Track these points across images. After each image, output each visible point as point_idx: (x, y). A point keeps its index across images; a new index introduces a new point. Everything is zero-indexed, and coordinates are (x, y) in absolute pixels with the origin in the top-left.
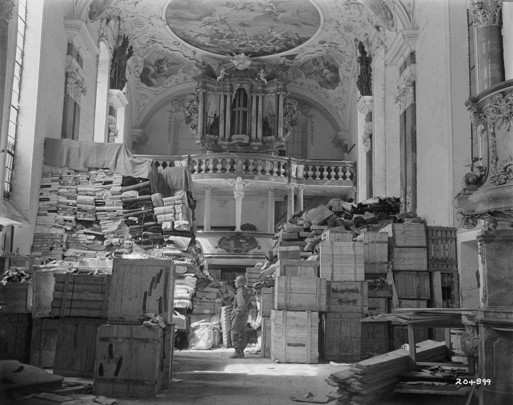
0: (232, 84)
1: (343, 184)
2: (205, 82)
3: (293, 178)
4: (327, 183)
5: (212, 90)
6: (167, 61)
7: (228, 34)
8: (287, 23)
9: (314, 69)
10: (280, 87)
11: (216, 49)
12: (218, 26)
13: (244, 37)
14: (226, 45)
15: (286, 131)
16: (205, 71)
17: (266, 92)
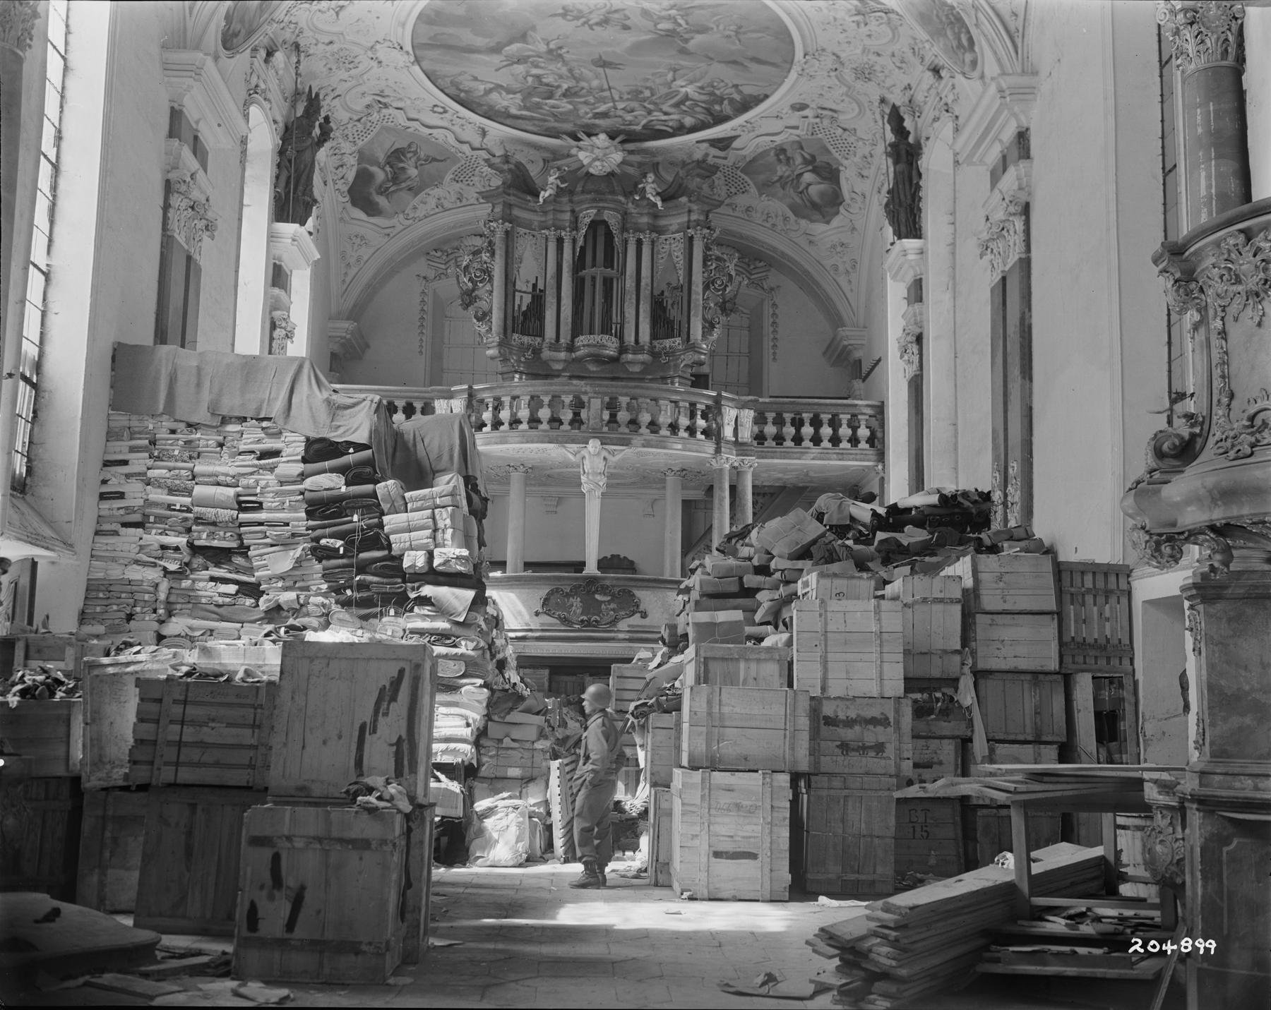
0: (577, 209)
1: (851, 457)
2: (510, 206)
3: (728, 442)
4: (812, 456)
5: (528, 225)
6: (415, 153)
7: (565, 86)
8: (711, 59)
9: (779, 173)
10: (694, 217)
11: (536, 122)
12: (542, 68)
13: (607, 94)
14: (561, 114)
15: (709, 326)
16: (509, 177)
17: (659, 231)
